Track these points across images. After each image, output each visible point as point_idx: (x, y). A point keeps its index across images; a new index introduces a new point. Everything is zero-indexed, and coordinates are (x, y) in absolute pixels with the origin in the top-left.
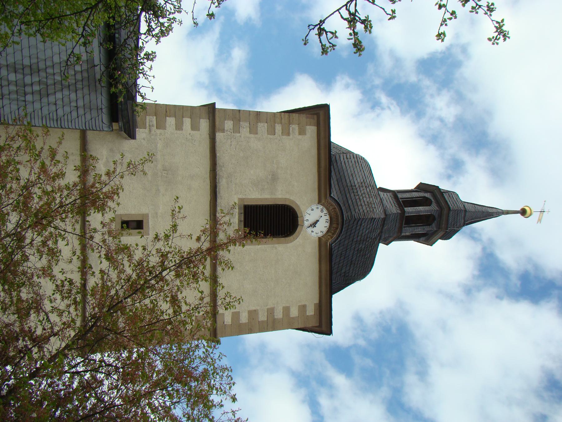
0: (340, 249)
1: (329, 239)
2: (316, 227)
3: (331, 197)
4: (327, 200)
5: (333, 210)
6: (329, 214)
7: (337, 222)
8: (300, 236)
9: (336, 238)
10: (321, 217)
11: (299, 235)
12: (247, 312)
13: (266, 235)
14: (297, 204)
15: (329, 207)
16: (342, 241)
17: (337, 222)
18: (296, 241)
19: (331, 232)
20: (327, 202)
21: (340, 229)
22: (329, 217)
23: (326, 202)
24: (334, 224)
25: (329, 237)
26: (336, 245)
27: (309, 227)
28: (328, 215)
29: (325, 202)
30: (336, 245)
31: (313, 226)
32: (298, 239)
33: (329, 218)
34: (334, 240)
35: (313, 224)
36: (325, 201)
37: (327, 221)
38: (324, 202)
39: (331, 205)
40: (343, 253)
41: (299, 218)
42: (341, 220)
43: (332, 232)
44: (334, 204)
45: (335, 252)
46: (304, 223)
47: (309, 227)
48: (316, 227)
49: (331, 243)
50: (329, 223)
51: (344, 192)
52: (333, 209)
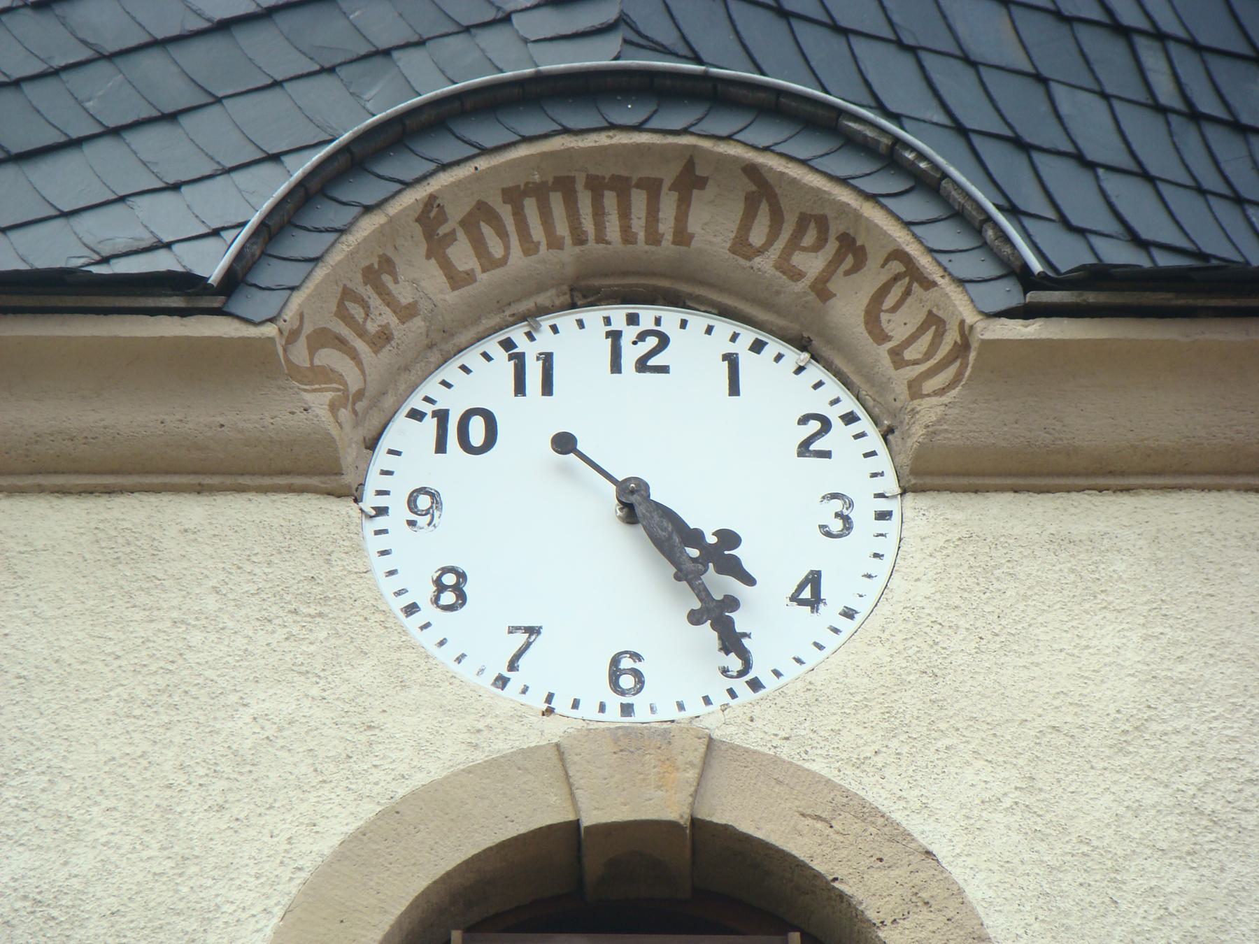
0: (1101, 146)
1: (934, 321)
2: (729, 538)
3: (234, 281)
4: (300, 355)
5: (462, 255)
6: (530, 317)
7: (653, 188)
8: (876, 794)
9: (915, 207)
10: (564, 443)
11: (867, 813)
12: (797, 214)
13: (1216, 316)
14: (361, 834)
15: (406, 313)
16: (977, 116)
17: (653, 188)
18: (957, 873)
19: (822, 290)
20: (323, 338)
21: (764, 134)
22: (566, 321)
23: (329, 357)
24: (682, 236)
25: (899, 325)
26: (1033, 201)
27: (732, 642)
28: (544, 340)
29: (324, 376)
30: (1037, 203)
31: (720, 584)
32: (924, 831)
33: (593, 317)
34: (947, 235)
35: (686, 574)
36: (324, 376)
37: (631, 353)
38: (319, 401)
39: (371, 276)
40: (1166, 93)
41: (591, 817)
42: (630, 113)
43: (812, 264)
44: (369, 225)
45: (1154, 226)
46: (663, 736)
47: (732, 642)
48: (729, 538)
49: (1008, 294)
50: (671, 318)
51: (151, 63)
52: (437, 246)
